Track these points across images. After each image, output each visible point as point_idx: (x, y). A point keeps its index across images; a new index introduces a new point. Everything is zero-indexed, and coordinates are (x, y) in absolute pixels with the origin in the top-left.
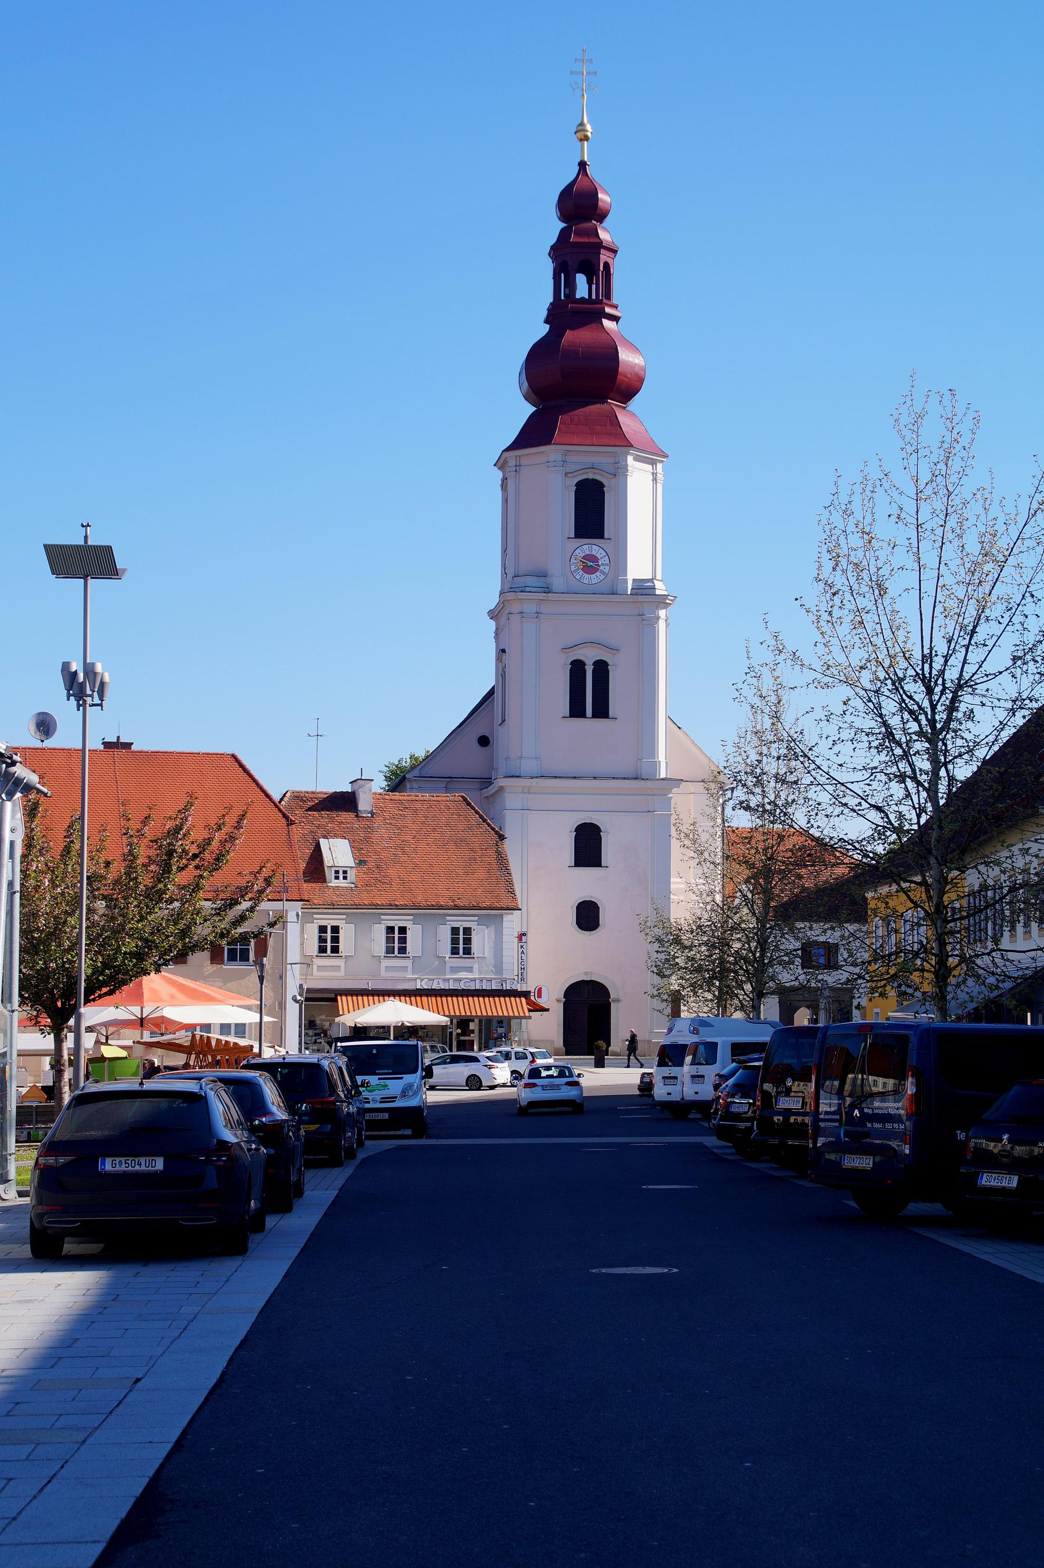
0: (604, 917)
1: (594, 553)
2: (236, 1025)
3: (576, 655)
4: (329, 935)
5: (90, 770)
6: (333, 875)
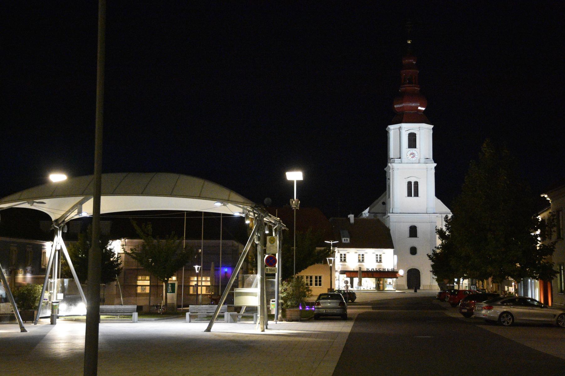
0: (409, 251)
2: (411, 196)
3: (409, 180)
6: (344, 240)
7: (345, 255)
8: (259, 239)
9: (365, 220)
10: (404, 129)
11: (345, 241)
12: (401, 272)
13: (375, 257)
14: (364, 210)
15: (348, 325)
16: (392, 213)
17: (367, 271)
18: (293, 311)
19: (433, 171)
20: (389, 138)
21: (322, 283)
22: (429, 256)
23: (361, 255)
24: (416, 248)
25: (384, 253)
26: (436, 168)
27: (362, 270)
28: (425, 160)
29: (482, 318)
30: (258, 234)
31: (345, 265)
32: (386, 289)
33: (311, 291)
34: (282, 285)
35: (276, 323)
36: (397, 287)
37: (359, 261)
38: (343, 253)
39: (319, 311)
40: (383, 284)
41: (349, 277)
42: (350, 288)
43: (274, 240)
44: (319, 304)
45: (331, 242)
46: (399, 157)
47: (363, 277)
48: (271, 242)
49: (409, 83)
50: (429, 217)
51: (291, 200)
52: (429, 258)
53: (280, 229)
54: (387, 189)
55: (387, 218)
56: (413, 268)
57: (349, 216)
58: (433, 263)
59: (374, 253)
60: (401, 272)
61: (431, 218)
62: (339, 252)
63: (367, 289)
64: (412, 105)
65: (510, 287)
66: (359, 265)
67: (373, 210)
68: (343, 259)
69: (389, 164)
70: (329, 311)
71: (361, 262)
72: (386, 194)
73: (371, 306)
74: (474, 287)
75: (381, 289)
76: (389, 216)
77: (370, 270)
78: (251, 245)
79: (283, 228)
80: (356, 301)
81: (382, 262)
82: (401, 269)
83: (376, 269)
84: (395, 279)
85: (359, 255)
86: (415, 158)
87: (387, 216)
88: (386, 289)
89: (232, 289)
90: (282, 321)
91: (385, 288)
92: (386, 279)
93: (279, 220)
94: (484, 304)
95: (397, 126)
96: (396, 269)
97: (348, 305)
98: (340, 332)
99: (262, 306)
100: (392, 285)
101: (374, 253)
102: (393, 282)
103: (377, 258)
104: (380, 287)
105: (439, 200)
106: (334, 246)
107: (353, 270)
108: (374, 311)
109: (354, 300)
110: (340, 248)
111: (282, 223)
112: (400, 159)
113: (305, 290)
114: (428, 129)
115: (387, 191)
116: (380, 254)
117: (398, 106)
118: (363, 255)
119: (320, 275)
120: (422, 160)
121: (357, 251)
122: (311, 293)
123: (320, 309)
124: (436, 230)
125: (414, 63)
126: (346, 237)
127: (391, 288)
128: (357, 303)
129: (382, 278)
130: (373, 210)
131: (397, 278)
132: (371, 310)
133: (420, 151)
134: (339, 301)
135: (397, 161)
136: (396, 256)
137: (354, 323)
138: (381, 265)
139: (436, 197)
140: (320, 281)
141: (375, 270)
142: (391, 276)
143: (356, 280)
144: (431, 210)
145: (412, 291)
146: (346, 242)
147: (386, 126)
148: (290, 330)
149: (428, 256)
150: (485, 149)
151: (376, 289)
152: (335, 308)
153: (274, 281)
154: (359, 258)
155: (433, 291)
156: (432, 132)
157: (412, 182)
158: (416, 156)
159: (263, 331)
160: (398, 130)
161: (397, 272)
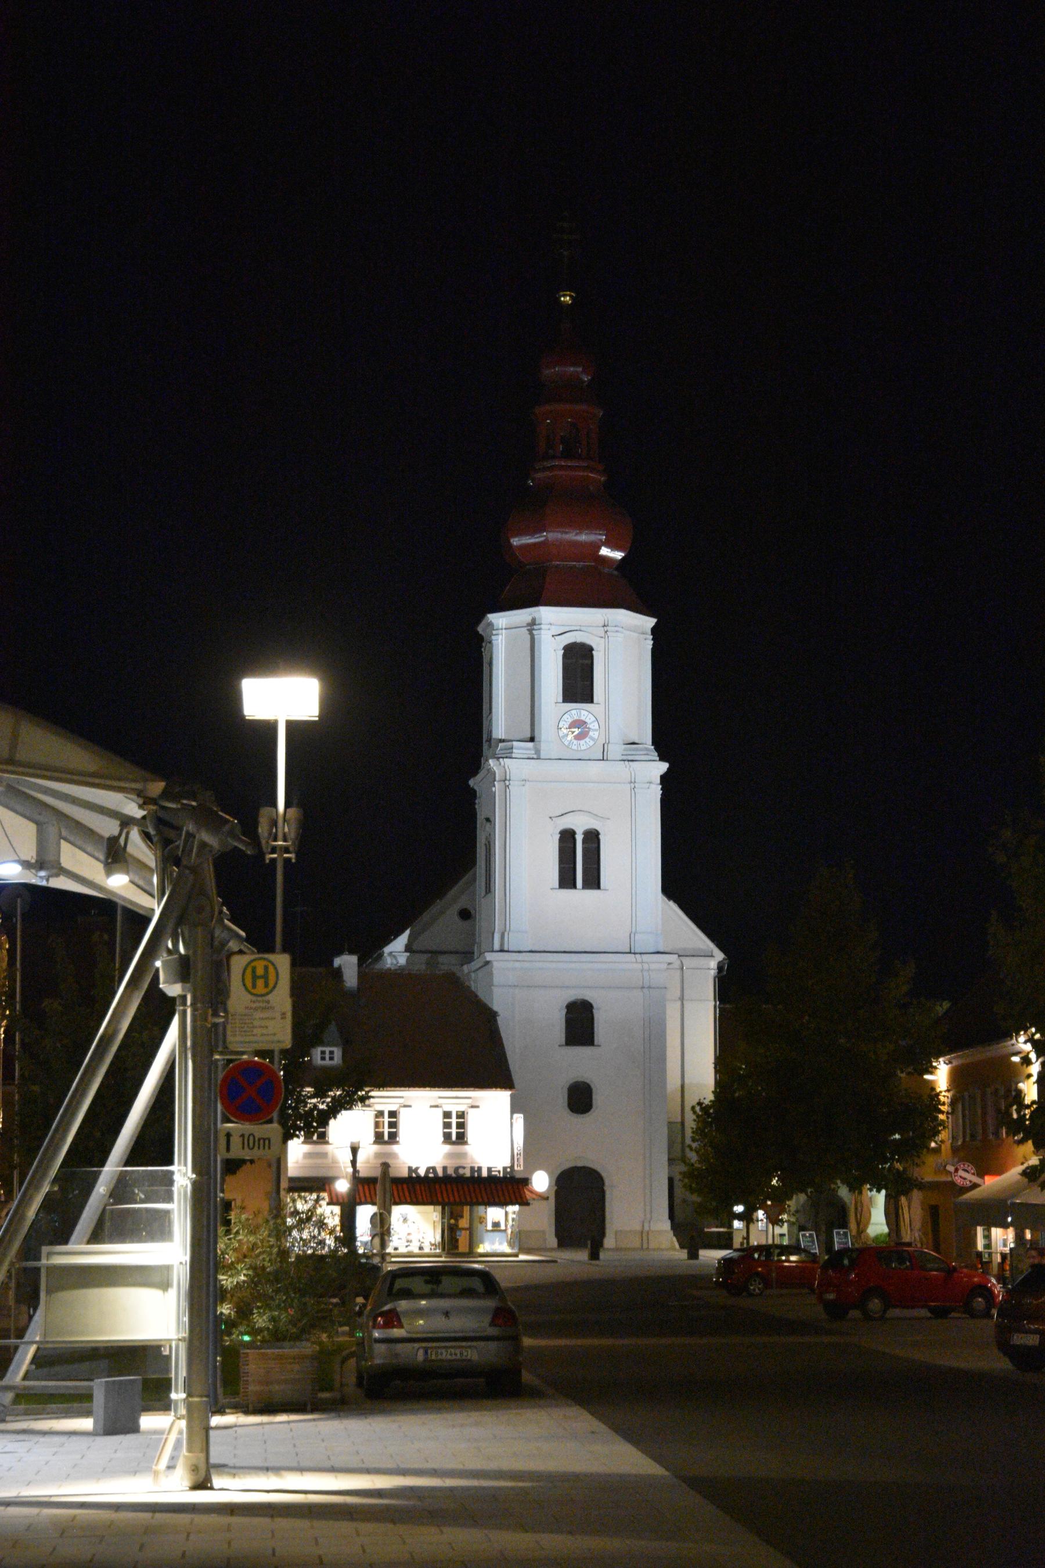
0: (562, 1099)
1: (583, 718)
2: (574, 886)
3: (567, 823)
8: (184, 970)
9: (398, 976)
10: (549, 626)
11: (323, 1059)
12: (541, 1182)
14: (388, 941)
16: (502, 951)
17: (410, 1178)
18: (280, 1357)
19: (656, 791)
20: (490, 664)
23: (386, 1115)
24: (592, 1086)
26: (664, 779)
27: (394, 1173)
28: (624, 750)
30: (176, 944)
31: (324, 1155)
32: (481, 1249)
36: (521, 1240)
39: (397, 1355)
40: (471, 1229)
43: (249, 983)
46: (529, 735)
48: (254, 986)
50: (639, 966)
55: (480, 973)
56: (580, 1164)
59: (437, 1106)
60: (541, 1182)
61: (649, 970)
63: (409, 1249)
65: (994, 1230)
66: (377, 1155)
67: (421, 943)
70: (447, 1354)
71: (386, 1143)
74: (811, 1236)
75: (463, 1247)
76: (487, 963)
77: (422, 1172)
78: (143, 999)
81: (466, 1143)
83: (445, 1168)
86: (587, 739)
88: (481, 1249)
89: (30, 1251)
92: (481, 1208)
95: (521, 616)
99: (197, 1343)
100: (505, 1231)
103: (447, 1125)
105: (671, 903)
112: (530, 745)
116: (461, 1108)
120: (616, 750)
123: (399, 1347)
127: (500, 1243)
130: (426, 941)
131: (523, 1202)
133: (607, 717)
135: (521, 748)
136: (519, 1119)
138: (464, 1155)
142: (502, 1198)
144: (645, 941)
145: (583, 1255)
148: (333, 1470)
151: (443, 1249)
152: (455, 1339)
153: (167, 1213)
154: (377, 1125)
155: (655, 1255)
156: (649, 644)
157: (577, 832)
158: (591, 733)
159: (203, 1484)
160: (524, 630)
161: (526, 1182)
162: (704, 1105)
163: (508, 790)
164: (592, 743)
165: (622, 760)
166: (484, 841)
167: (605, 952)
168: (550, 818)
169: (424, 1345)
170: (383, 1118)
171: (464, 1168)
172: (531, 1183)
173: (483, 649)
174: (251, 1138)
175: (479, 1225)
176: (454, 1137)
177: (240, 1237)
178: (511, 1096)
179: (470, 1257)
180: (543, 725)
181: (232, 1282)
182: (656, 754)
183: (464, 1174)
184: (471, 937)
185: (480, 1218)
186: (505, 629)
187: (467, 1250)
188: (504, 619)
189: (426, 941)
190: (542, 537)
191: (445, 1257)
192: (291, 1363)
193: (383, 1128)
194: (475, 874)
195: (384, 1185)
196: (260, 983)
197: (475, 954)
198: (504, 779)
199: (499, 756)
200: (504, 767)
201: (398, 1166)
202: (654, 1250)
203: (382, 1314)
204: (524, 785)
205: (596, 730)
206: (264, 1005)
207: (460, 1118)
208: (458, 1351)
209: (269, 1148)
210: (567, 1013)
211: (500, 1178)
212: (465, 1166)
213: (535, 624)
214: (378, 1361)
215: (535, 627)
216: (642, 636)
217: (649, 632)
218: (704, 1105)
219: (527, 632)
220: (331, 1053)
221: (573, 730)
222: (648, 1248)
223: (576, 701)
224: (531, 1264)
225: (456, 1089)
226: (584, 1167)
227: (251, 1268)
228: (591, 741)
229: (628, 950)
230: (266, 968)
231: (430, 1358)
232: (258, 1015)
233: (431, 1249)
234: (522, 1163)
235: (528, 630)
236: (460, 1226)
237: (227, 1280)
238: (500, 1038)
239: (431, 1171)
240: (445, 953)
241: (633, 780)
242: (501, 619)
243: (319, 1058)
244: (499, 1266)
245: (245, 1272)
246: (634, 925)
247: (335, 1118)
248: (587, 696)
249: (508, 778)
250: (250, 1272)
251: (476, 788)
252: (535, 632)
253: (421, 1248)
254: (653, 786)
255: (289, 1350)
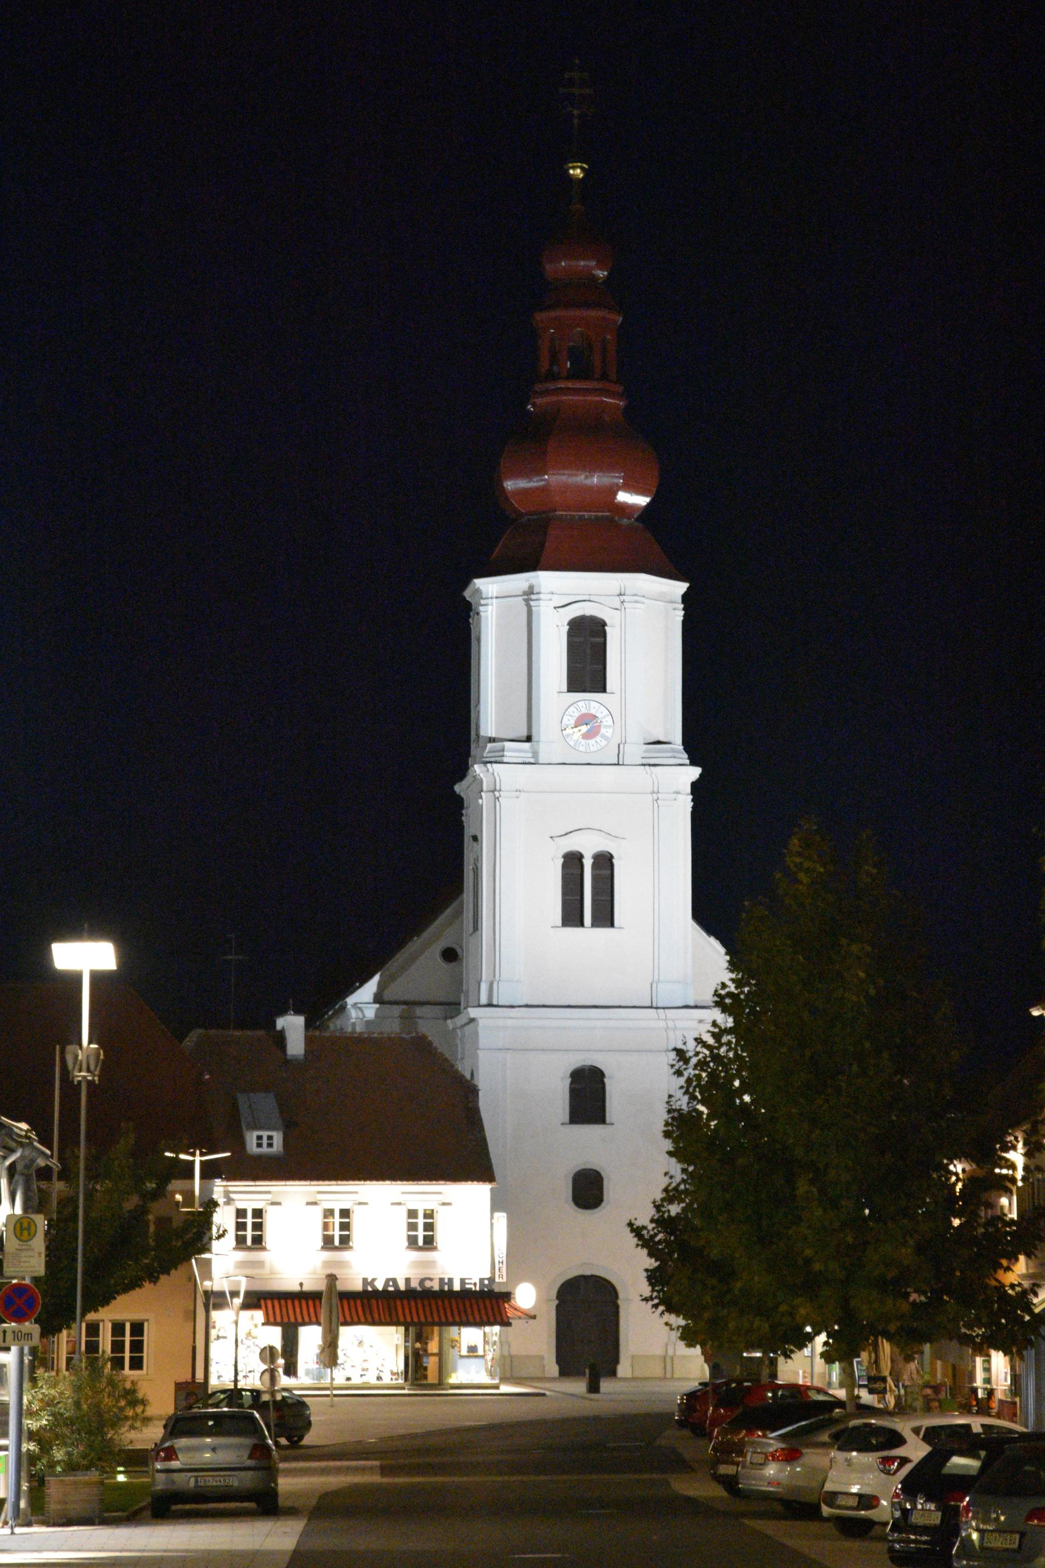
0: (566, 1190)
1: (593, 712)
2: (581, 924)
3: (572, 844)
4: (249, 1220)
5: (60, 1135)
6: (255, 1141)
7: (258, 1213)
10: (549, 596)
11: (259, 1145)
13: (403, 1220)
14: (351, 989)
15: (284, 1529)
16: (490, 1005)
17: (365, 1292)
18: (75, 1483)
19: (685, 804)
20: (479, 640)
21: (145, 1355)
22: (637, 1231)
23: (337, 1214)
24: (603, 1174)
25: (449, 1204)
26: (696, 788)
27: (341, 1286)
28: (646, 751)
29: (765, 1496)
31: (260, 1264)
32: (454, 1379)
33: (144, 1402)
34: (34, 1380)
35: (13, 1533)
37: (328, 1243)
38: (250, 1206)
39: (173, 1482)
40: (440, 1354)
41: (275, 1324)
42: (284, 1381)
43: (33, 1228)
44: (171, 1454)
45: (193, 1154)
46: (524, 733)
47: (346, 1323)
48: (21, 1234)
49: (572, 376)
51: (65, 1042)
52: (635, 1240)
53: (27, 1167)
54: (467, 896)
55: (467, 1028)
56: (588, 1272)
57: (281, 1022)
58: (652, 1263)
59: (399, 1204)
62: (229, 1201)
63: (364, 1379)
64: (588, 482)
66: (327, 1264)
67: (395, 991)
68: (249, 1233)
69: (478, 768)
70: (212, 1481)
71: (336, 1249)
72: (459, 912)
73: (377, 1463)
75: (432, 1377)
76: (472, 1020)
77: (380, 1286)
79: (41, 1162)
80: (308, 1439)
81: (435, 1249)
82: (530, 1280)
83: (408, 1281)
84: (497, 1329)
85: (329, 1213)
86: (598, 738)
87: (465, 1021)
88: (454, 1379)
90: (29, 1524)
91: (449, 1375)
92: (454, 1329)
93: (27, 1131)
94: (772, 1441)
96: (505, 1280)
97: (285, 1459)
98: (258, 1551)
100: (483, 1357)
101: (399, 1204)
102: (486, 1342)
103: (412, 1227)
104: (426, 1369)
105: (712, 940)
106: (210, 1171)
107: (297, 1288)
108: (386, 1480)
109: (301, 1438)
110: (235, 1179)
111: (39, 1142)
112: (527, 745)
113: (123, 1403)
114: (659, 598)
115: (465, 895)
117: (523, 484)
118: (345, 1213)
119: (136, 1316)
120: (635, 752)
121: (320, 1197)
122: (143, 1412)
123: (176, 1475)
124: (669, 1112)
125: (602, 274)
126: (261, 1128)
128: (311, 1452)
129: (433, 1324)
130: (403, 988)
131: (505, 1323)
132: (377, 1479)
134: (248, 1441)
137: (307, 1525)
138: (431, 1264)
139: (695, 925)
140: (137, 1347)
141: (402, 1287)
143: (311, 1337)
145: (578, 1386)
146: (265, 1149)
147: (466, 583)
149: (632, 1231)
150: (798, 860)
151: (406, 1379)
152: (221, 1469)
154: (326, 1227)
156: (679, 615)
158: (603, 731)
161: (507, 1296)
162: (635, 1227)
163: (498, 803)
164: (604, 743)
165: (643, 765)
166: (472, 861)
167: (620, 1007)
168: (551, 837)
169: (196, 1474)
170: (334, 1218)
171: (431, 1279)
172: (514, 1298)
173: (471, 621)
174: (20, 1334)
175: (451, 1350)
176: (421, 1242)
177: (44, 1391)
178: (492, 1190)
179: (439, 1390)
180: (543, 715)
181: (37, 1426)
182: (686, 756)
183: (432, 1287)
184: (458, 983)
185: (452, 1341)
186: (497, 598)
187: (436, 1382)
188: (495, 585)
189: (403, 988)
190: (542, 480)
191: (409, 1389)
192: (83, 1488)
193: (334, 1230)
194: (462, 902)
195: (330, 1299)
196: (26, 1233)
197: (462, 1004)
198: (493, 789)
199: (488, 760)
200: (493, 774)
201: (350, 1277)
202: (679, 1379)
203: (163, 1450)
204: (518, 797)
205: (609, 726)
206: (29, 1247)
207: (429, 1218)
208: (222, 1479)
209: (31, 1339)
210: (572, 1083)
211: (476, 1291)
212: (432, 1277)
213: (532, 593)
214: (159, 1488)
215: (533, 597)
216: (670, 605)
217: (680, 600)
218: (635, 1227)
219: (523, 603)
220: (270, 1138)
221: (579, 728)
222: (672, 1378)
223: (584, 690)
224: (508, 1397)
225: (423, 1182)
226: (592, 1276)
227: (53, 1415)
228: (603, 741)
229: (649, 1004)
230: (21, 1234)
231: (199, 1484)
232: (23, 1254)
233: (392, 1379)
234: (504, 1273)
235: (524, 600)
236: (430, 1351)
237: (32, 1424)
238: (480, 1119)
239: (391, 1283)
240: (422, 1004)
241: (656, 790)
242: (490, 585)
243: (255, 1145)
244: (472, 1401)
245: (46, 1417)
246: (656, 972)
247: (176, 1269)
248: (599, 684)
249: (498, 788)
250: (50, 1418)
251: (462, 794)
252: (532, 603)
253: (379, 1378)
254: (681, 797)
255: (81, 1477)
